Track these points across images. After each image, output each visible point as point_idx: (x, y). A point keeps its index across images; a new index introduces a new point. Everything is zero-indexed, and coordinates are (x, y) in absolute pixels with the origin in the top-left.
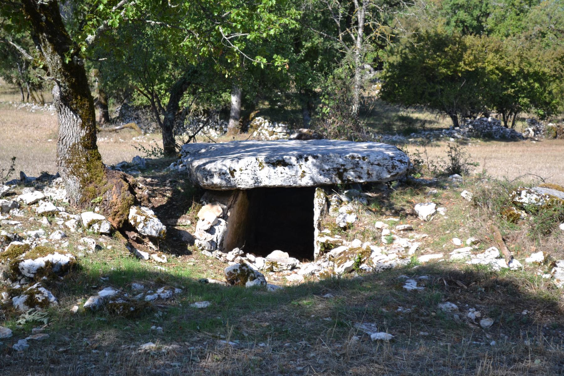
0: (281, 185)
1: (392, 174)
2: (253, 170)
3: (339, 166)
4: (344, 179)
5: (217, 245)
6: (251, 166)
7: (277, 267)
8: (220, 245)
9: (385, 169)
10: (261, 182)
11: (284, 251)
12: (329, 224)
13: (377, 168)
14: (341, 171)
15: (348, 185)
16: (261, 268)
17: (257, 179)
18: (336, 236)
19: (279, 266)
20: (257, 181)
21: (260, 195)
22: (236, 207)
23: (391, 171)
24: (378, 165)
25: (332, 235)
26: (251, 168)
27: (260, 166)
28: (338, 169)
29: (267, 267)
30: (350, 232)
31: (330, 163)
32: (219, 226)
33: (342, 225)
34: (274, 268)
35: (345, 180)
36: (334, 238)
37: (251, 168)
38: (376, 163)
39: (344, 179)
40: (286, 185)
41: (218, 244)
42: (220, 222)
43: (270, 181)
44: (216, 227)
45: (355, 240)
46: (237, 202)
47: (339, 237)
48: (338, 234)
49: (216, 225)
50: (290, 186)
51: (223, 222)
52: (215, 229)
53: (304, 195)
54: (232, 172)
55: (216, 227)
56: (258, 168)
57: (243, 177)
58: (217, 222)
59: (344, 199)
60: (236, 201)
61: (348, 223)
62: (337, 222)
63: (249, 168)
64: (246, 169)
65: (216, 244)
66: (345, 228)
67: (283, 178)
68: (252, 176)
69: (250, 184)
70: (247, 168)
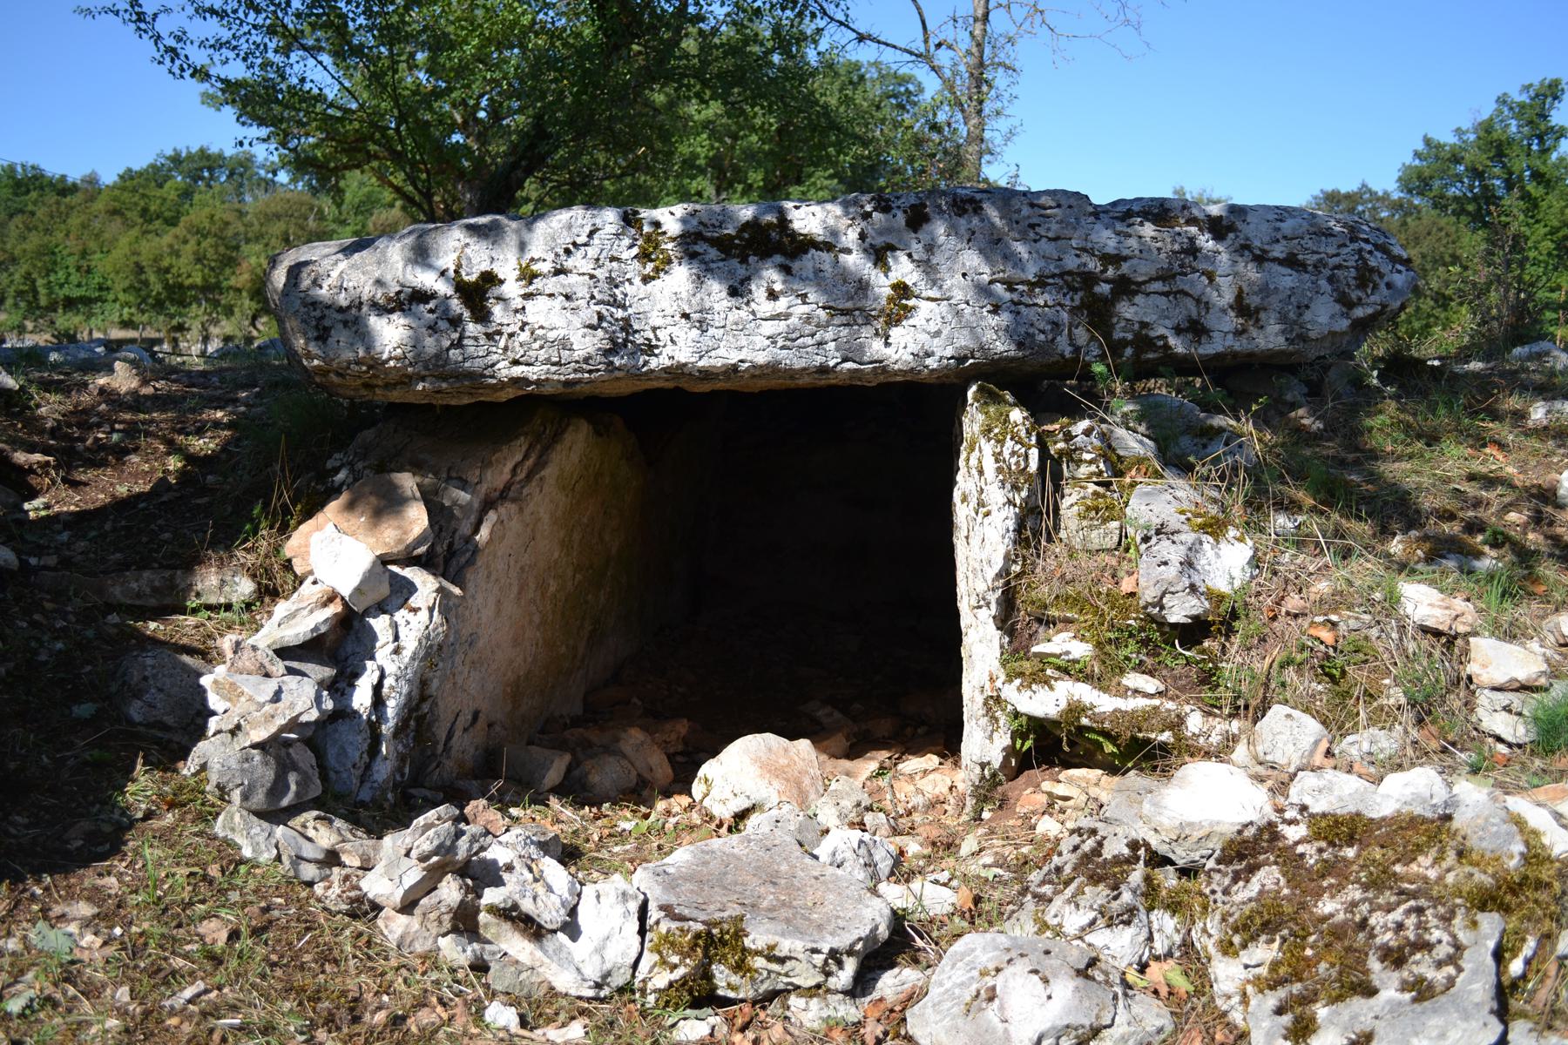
0: (772, 369)
1: (1359, 312)
2: (601, 274)
3: (1093, 265)
4: (1118, 335)
5: (376, 739)
6: (592, 252)
7: (740, 967)
8: (398, 732)
9: (1323, 283)
10: (650, 349)
11: (792, 737)
12: (1075, 602)
13: (1286, 279)
14: (1104, 288)
15: (1143, 361)
16: (618, 980)
17: (626, 326)
18: (1133, 680)
19: (759, 962)
20: (623, 338)
21: (645, 419)
22: (545, 500)
23: (1354, 295)
24: (1291, 262)
25: (1102, 675)
26: (587, 267)
27: (644, 256)
28: (1089, 279)
29: (662, 980)
30: (1237, 661)
31: (1044, 245)
32: (401, 615)
33: (1179, 611)
34: (722, 976)
35: (1124, 343)
36: (1124, 692)
37: (587, 267)
38: (1278, 251)
39: (1118, 335)
40: (799, 364)
41: (387, 729)
42: (404, 590)
43: (707, 341)
44: (380, 624)
45: (1277, 711)
46: (549, 472)
47: (1150, 684)
48: (1140, 668)
49: (382, 608)
50: (823, 370)
51: (425, 585)
52: (373, 637)
53: (909, 424)
54: (477, 294)
55: (380, 624)
56: (634, 269)
57: (538, 312)
58: (385, 590)
59: (1133, 443)
60: (540, 464)
61: (1217, 598)
62: (1149, 594)
63: (577, 262)
64: (559, 272)
65: (374, 728)
66: (1194, 632)
67: (781, 326)
68: (589, 313)
69: (579, 354)
70: (569, 263)
